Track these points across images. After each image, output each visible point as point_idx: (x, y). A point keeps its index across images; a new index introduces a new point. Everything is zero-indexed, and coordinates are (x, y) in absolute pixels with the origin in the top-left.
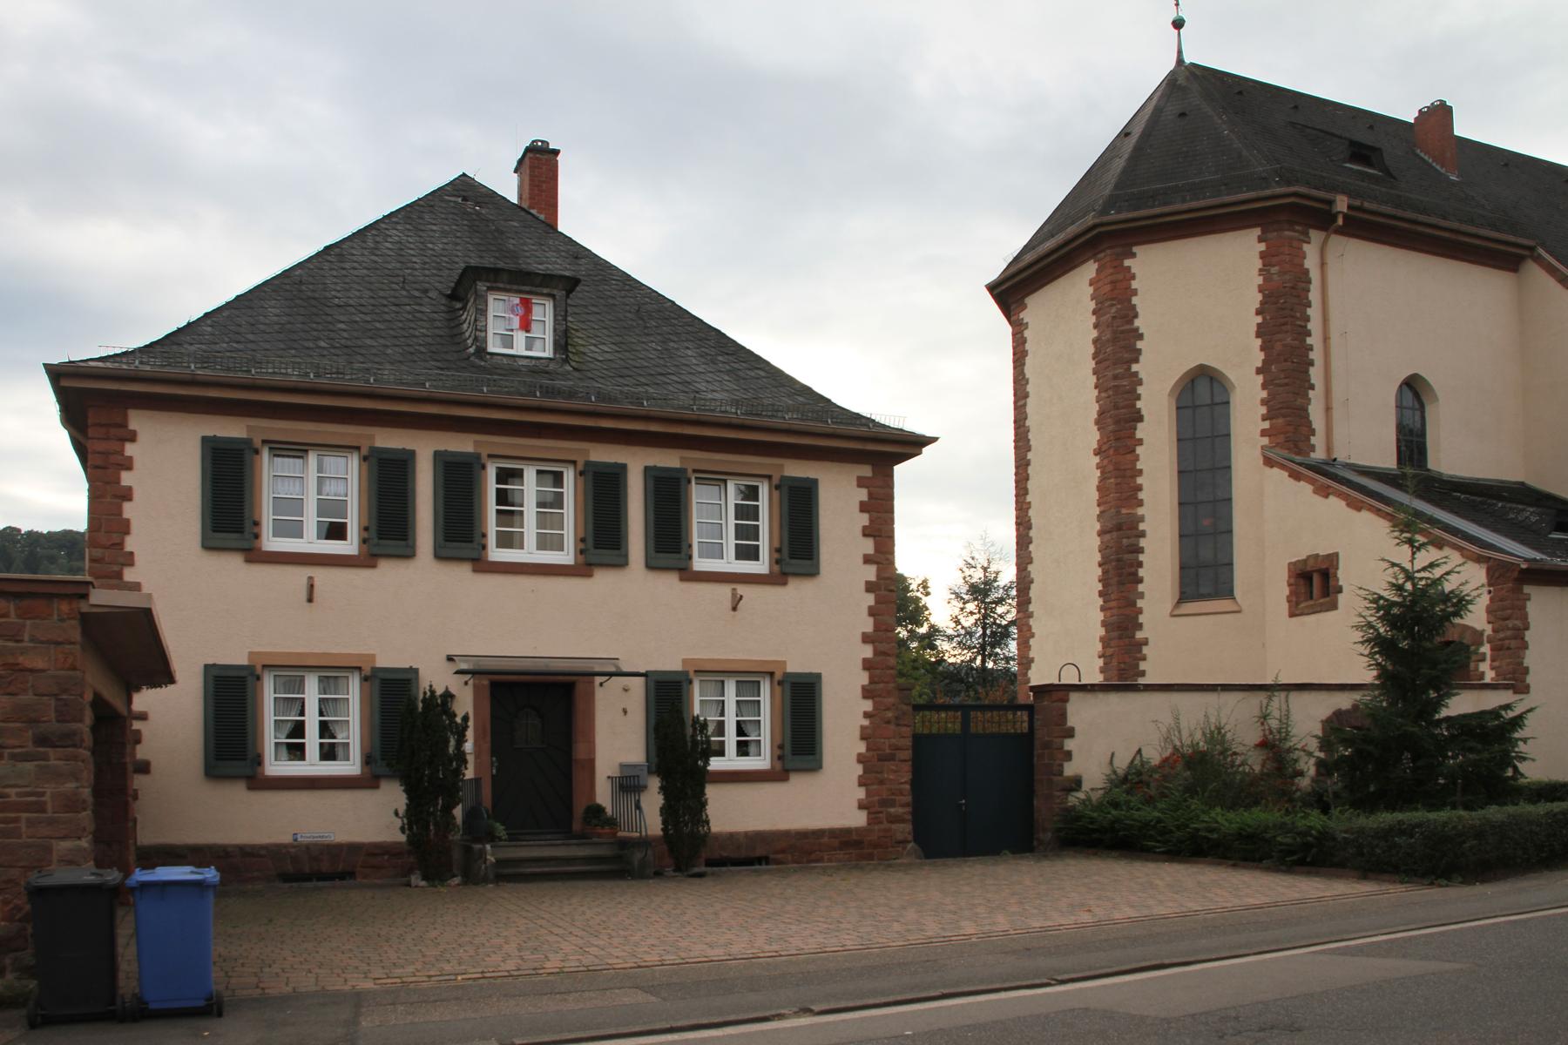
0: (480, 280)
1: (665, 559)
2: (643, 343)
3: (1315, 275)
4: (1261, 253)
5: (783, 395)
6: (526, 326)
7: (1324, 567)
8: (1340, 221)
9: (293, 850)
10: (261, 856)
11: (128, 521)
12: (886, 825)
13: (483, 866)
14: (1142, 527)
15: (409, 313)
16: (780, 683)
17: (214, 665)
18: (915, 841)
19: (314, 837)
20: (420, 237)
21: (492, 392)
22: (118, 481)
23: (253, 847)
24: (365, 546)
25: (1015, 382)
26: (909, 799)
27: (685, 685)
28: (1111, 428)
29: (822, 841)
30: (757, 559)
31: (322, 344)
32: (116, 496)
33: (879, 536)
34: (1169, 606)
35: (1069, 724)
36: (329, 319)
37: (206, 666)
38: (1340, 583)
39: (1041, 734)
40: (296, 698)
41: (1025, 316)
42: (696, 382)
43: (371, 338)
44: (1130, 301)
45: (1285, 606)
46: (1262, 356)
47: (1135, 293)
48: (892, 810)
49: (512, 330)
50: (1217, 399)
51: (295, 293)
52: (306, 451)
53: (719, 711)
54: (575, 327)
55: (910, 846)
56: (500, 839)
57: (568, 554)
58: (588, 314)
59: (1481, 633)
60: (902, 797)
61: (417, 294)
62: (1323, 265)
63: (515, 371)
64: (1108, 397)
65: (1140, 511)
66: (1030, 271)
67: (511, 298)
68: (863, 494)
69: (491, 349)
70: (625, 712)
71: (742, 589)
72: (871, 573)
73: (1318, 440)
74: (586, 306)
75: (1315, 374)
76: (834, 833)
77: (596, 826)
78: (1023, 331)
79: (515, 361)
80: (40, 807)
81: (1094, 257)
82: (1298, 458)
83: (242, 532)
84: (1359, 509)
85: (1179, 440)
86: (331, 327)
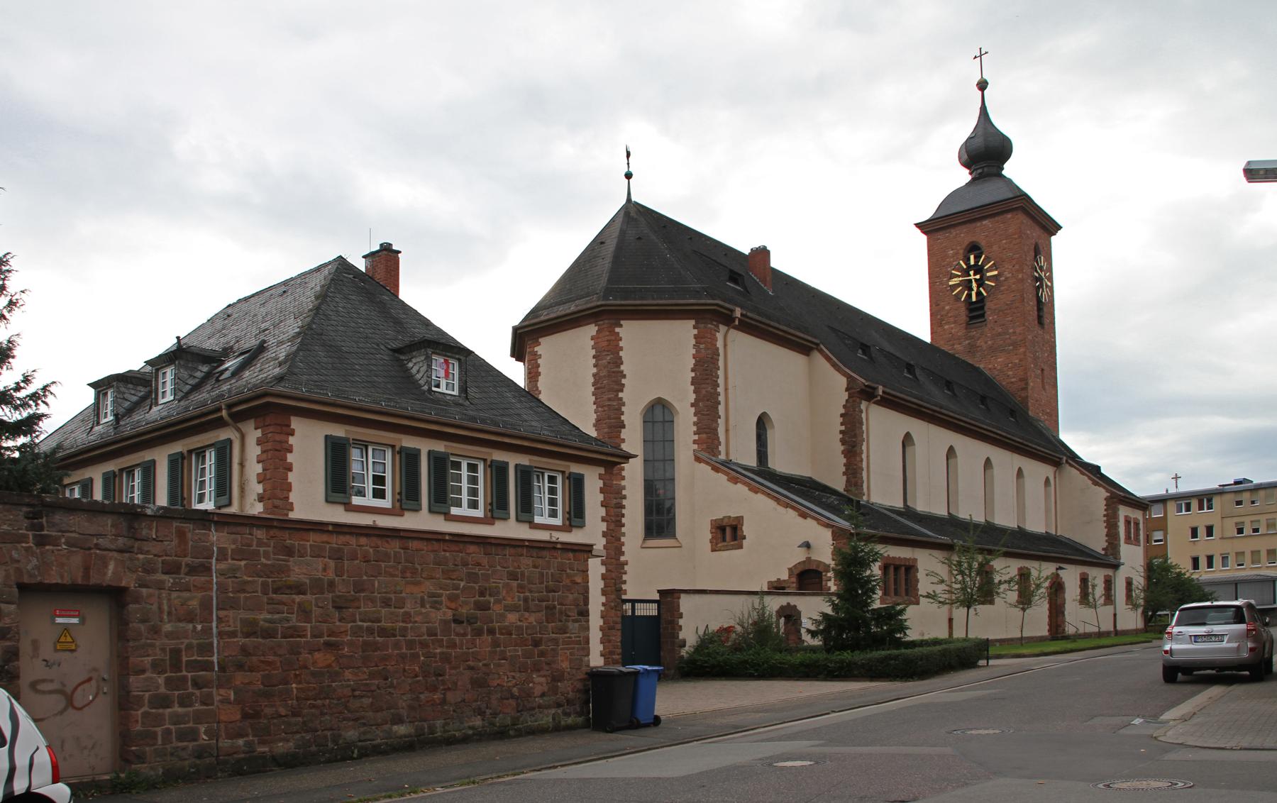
1: (525, 516)
3: (721, 351)
4: (695, 335)
7: (734, 523)
8: (737, 323)
14: (624, 492)
21: (388, 406)
28: (606, 430)
30: (384, 498)
34: (641, 542)
38: (744, 534)
44: (618, 353)
45: (709, 545)
46: (694, 396)
47: (621, 349)
48: (614, 657)
49: (439, 378)
50: (667, 419)
59: (829, 566)
62: (725, 345)
64: (604, 411)
65: (623, 483)
73: (722, 448)
75: (721, 408)
81: (596, 323)
82: (714, 458)
84: (756, 492)
85: (644, 441)
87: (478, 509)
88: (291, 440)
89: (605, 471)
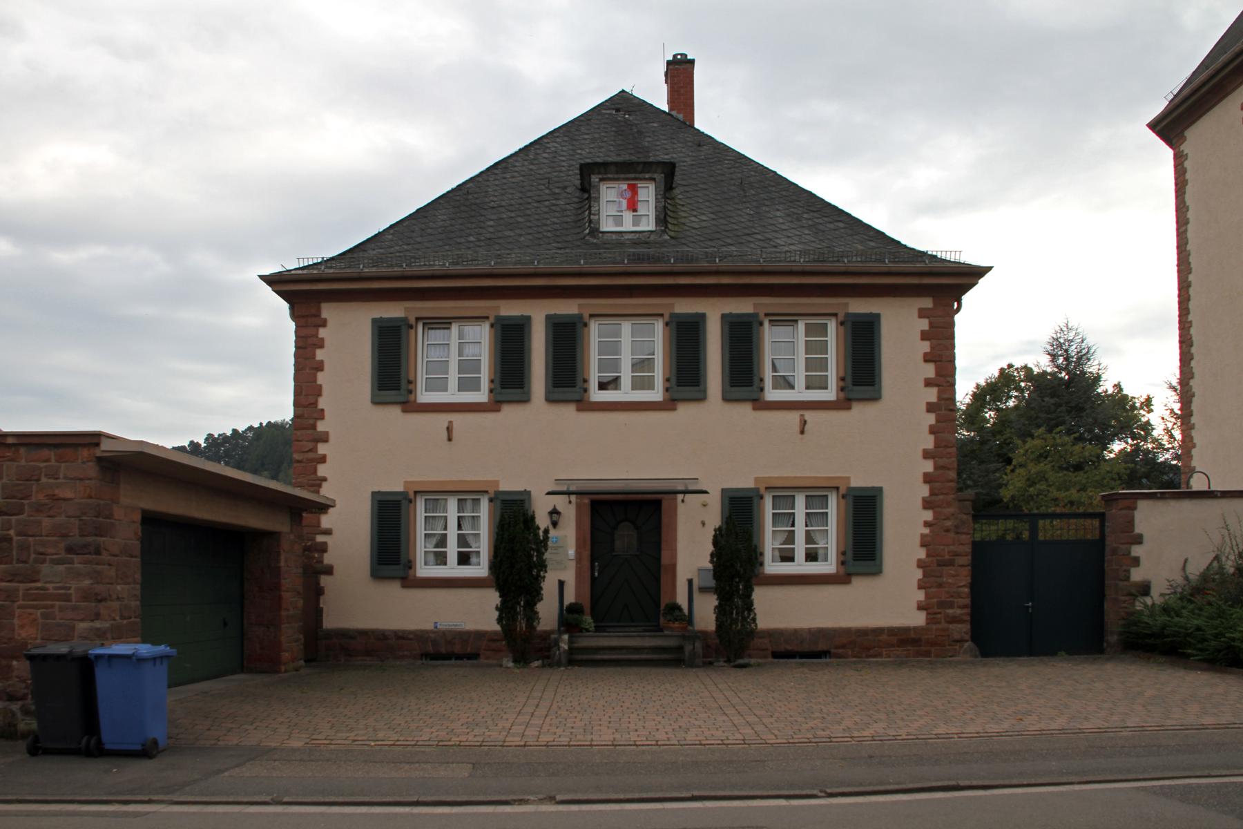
0: (593, 174)
2: (739, 210)
5: (856, 241)
6: (633, 206)
9: (432, 635)
10: (411, 639)
11: (320, 387)
12: (944, 625)
13: (558, 652)
15: (547, 207)
16: (844, 497)
17: (379, 492)
18: (972, 641)
19: (449, 625)
20: (573, 145)
22: (314, 355)
23: (404, 632)
24: (492, 395)
25: (1176, 211)
26: (968, 601)
27: (755, 500)
29: (881, 638)
30: (479, 390)
31: (472, 239)
32: (312, 368)
33: (941, 361)
35: (1137, 530)
36: (482, 218)
37: (723, 490)
39: (1110, 541)
40: (442, 516)
41: (1186, 148)
42: (777, 238)
43: (511, 230)
48: (950, 611)
49: (622, 211)
51: (462, 202)
52: (450, 323)
53: (791, 523)
54: (682, 203)
55: (966, 645)
56: (587, 630)
57: (658, 392)
58: (697, 190)
60: (960, 600)
61: (557, 191)
63: (621, 244)
66: (1193, 98)
67: (621, 186)
68: (924, 324)
69: (604, 228)
70: (703, 524)
71: (809, 415)
72: (932, 395)
74: (696, 185)
76: (892, 631)
77: (670, 620)
78: (1183, 162)
79: (622, 236)
80: (67, 598)
83: (399, 390)
86: (482, 225)
87: (654, 389)
88: (322, 333)
89: (935, 304)
